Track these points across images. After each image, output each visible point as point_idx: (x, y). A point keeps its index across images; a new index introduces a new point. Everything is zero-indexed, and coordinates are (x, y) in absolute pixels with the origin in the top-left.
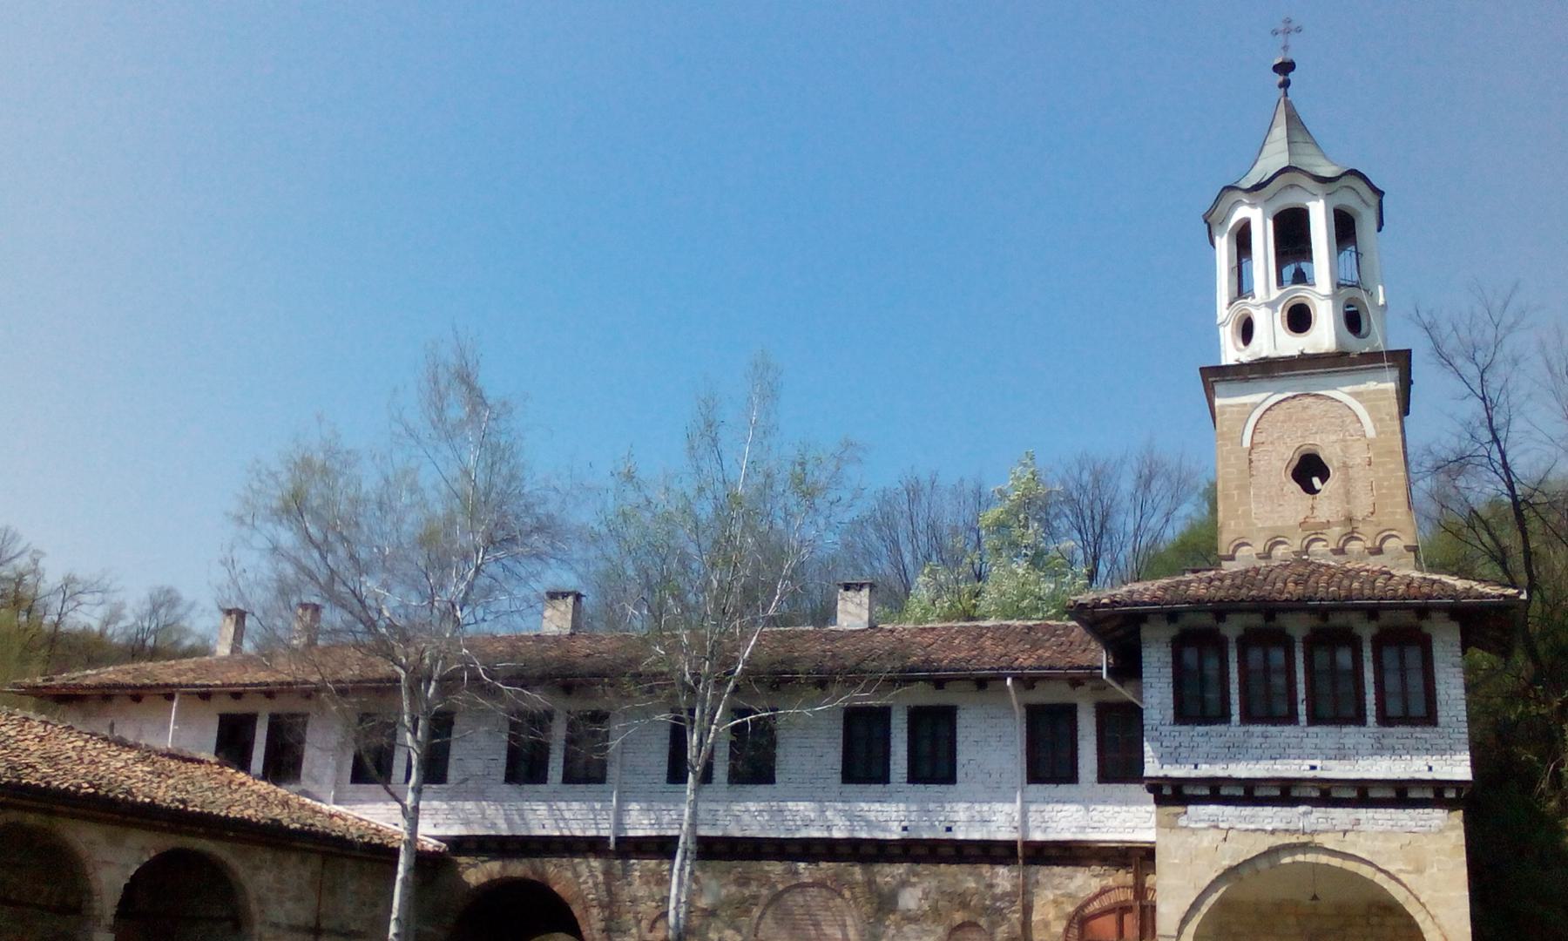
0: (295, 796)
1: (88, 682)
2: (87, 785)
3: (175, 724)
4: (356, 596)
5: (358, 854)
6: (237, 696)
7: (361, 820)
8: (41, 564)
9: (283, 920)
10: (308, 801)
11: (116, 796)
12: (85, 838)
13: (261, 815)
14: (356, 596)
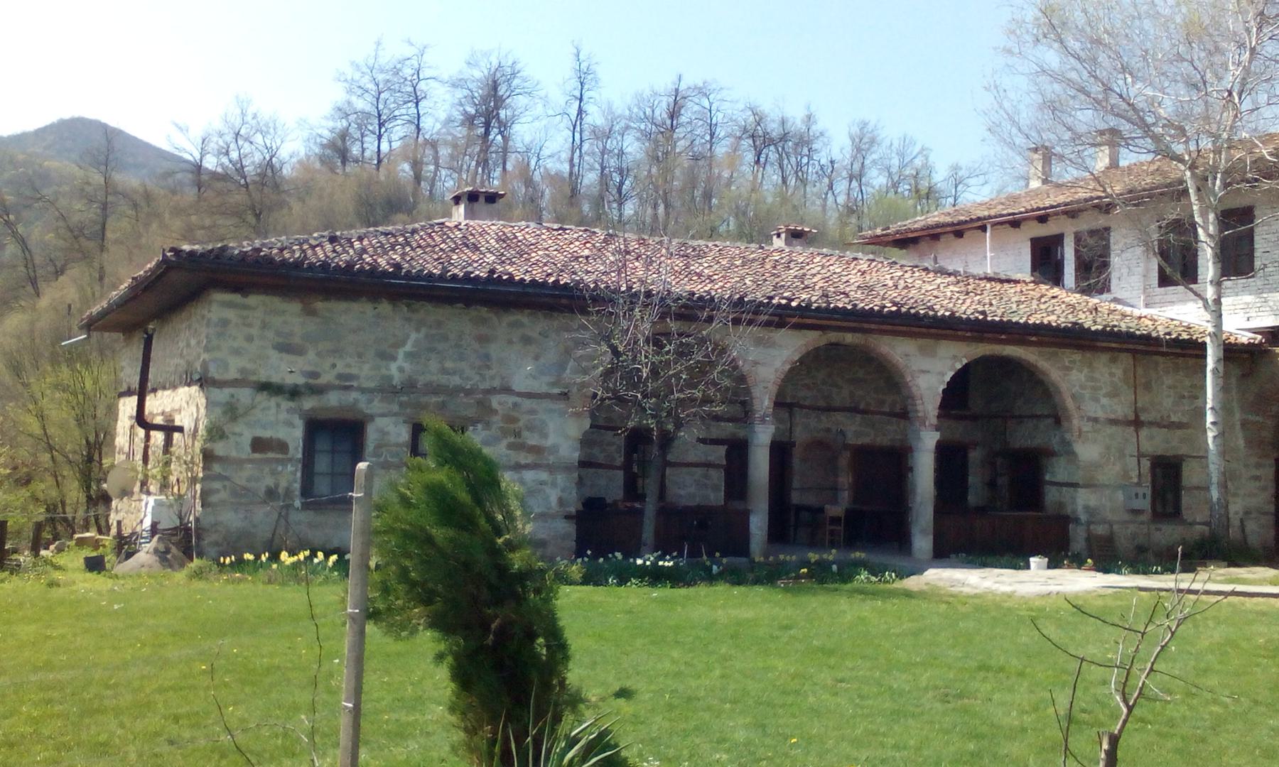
0: (1107, 303)
1: (916, 226)
2: (890, 305)
3: (991, 251)
4: (1124, 99)
5: (1164, 349)
6: (1043, 219)
7: (1172, 320)
8: (931, 159)
9: (1100, 414)
10: (1119, 307)
11: (917, 313)
12: (899, 351)
13: (1063, 320)
14: (1124, 99)
